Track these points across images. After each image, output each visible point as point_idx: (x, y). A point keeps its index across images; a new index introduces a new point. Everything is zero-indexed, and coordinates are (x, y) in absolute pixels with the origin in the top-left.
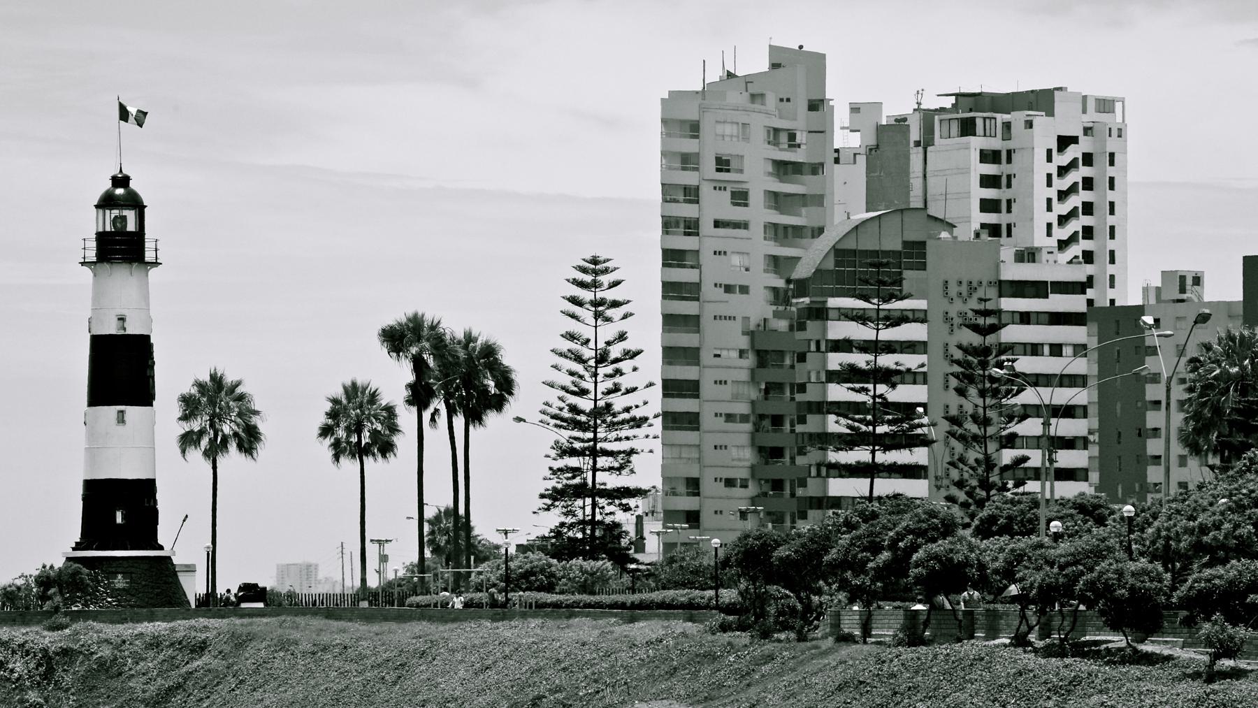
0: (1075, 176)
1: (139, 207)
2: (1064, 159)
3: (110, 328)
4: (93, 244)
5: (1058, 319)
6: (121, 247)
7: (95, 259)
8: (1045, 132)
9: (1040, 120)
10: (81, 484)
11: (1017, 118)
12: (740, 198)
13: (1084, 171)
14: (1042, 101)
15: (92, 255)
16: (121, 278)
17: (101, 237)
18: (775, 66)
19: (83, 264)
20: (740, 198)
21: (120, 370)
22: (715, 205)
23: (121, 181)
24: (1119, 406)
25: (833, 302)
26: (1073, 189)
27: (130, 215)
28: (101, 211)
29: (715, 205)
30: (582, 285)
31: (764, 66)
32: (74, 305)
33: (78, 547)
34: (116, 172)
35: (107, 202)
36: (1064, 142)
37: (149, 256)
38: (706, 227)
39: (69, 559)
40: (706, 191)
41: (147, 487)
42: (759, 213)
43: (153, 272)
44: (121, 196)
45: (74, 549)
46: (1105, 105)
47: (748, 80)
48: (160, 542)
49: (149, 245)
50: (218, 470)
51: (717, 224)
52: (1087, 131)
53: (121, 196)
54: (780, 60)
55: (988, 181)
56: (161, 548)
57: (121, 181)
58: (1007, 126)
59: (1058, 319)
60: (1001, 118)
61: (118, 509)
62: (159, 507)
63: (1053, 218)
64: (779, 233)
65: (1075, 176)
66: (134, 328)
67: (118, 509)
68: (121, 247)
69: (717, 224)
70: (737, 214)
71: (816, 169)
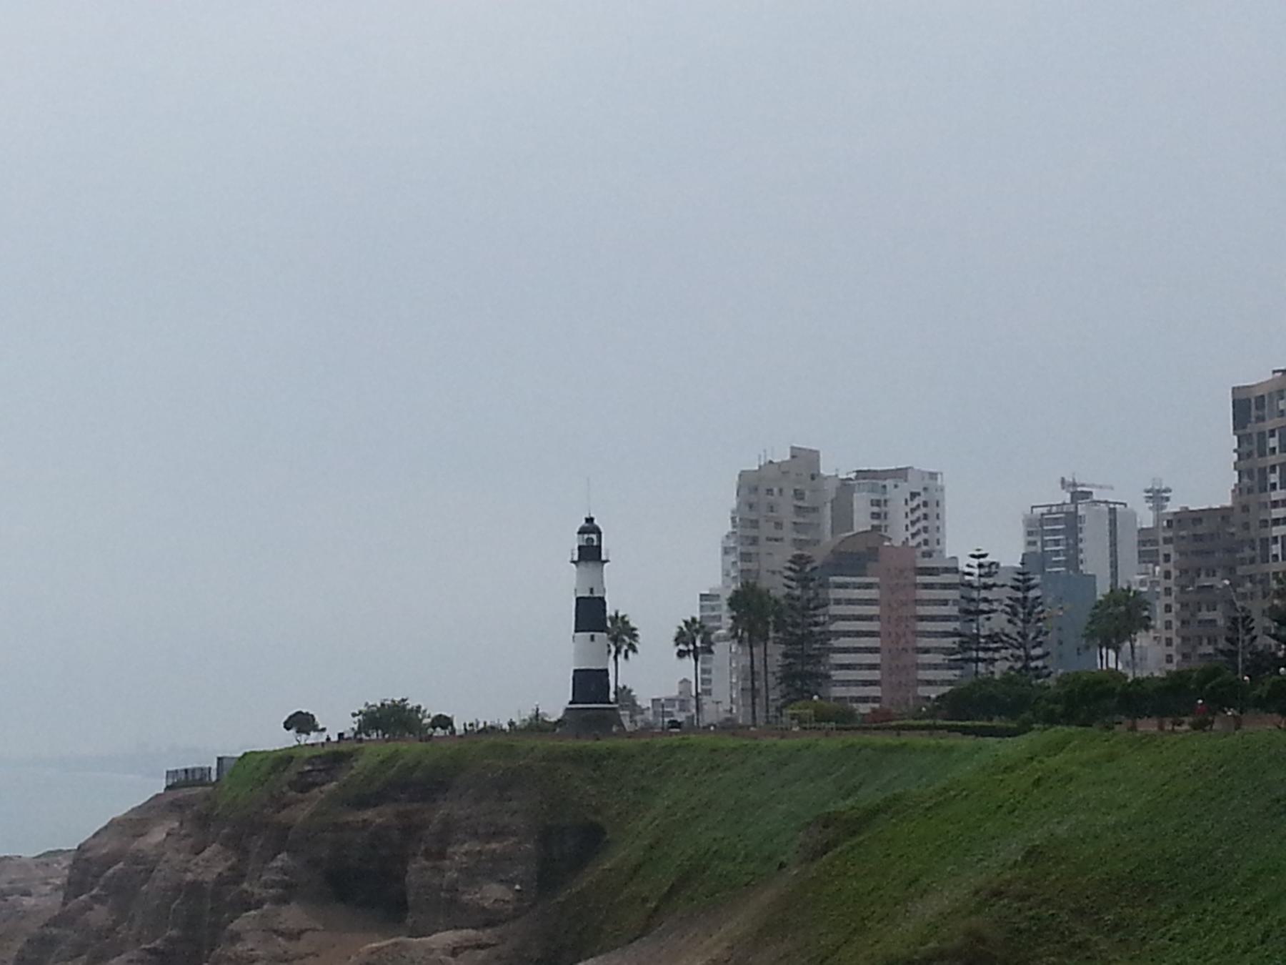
0: (919, 513)
1: (599, 533)
2: (914, 504)
4: (576, 552)
5: (945, 586)
6: (590, 554)
8: (905, 488)
9: (901, 484)
11: (889, 483)
12: (779, 525)
13: (923, 510)
14: (901, 474)
15: (576, 558)
18: (793, 457)
20: (779, 525)
21: (590, 613)
22: (767, 530)
23: (590, 520)
25: (832, 579)
26: (918, 520)
27: (594, 536)
29: (767, 530)
30: (1017, 580)
31: (788, 458)
32: (567, 584)
36: (913, 495)
37: (604, 558)
38: (762, 540)
40: (762, 522)
42: (788, 534)
43: (606, 565)
44: (590, 528)
46: (933, 476)
47: (779, 464)
51: (769, 539)
52: (925, 489)
53: (590, 528)
54: (796, 453)
55: (875, 516)
58: (884, 487)
59: (945, 586)
60: (881, 483)
63: (908, 535)
64: (798, 543)
65: (919, 513)
67: (590, 683)
68: (590, 554)
69: (769, 539)
70: (779, 534)
71: (815, 510)
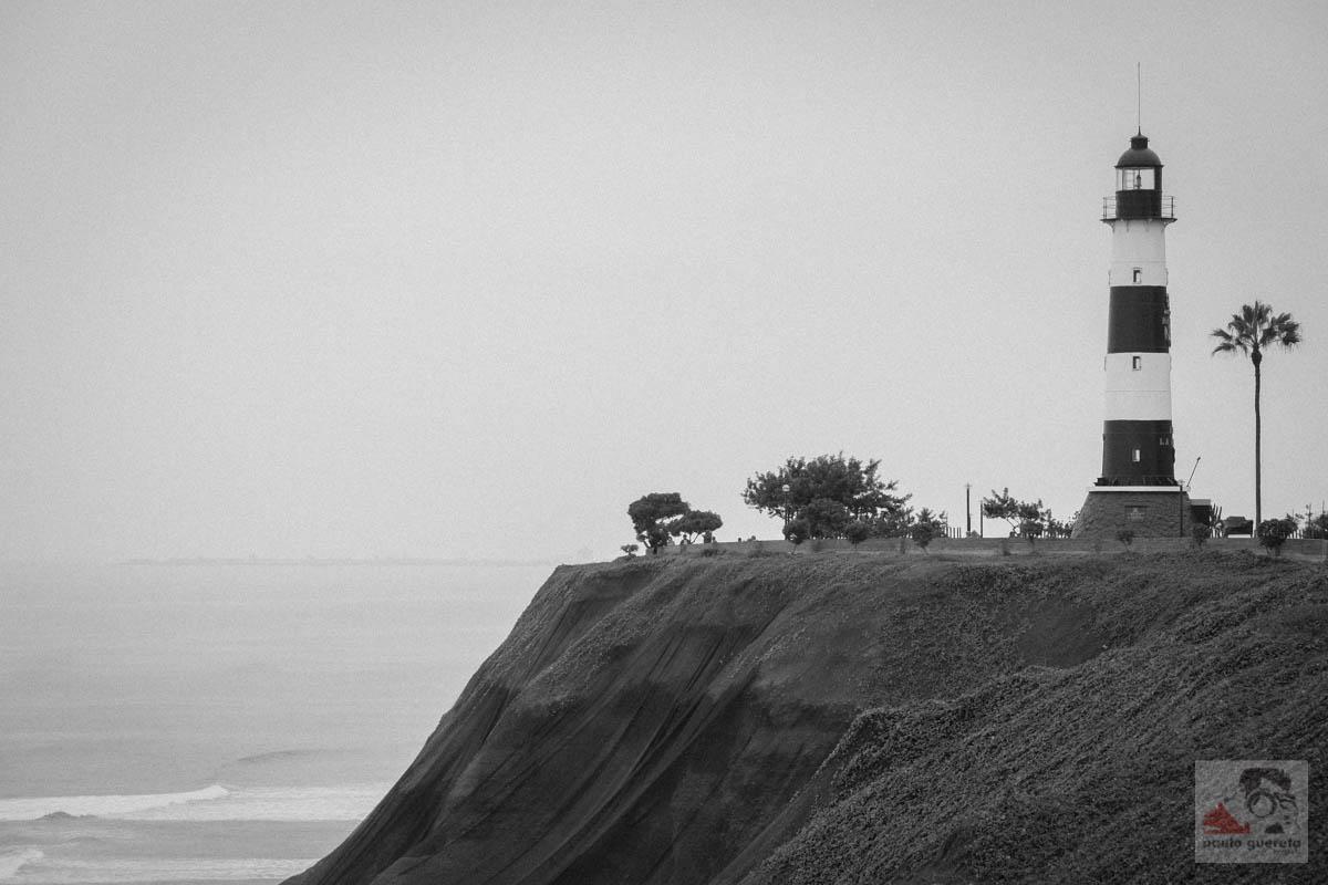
1: (1158, 168)
3: (1148, 359)
7: (1114, 216)
10: (1101, 430)
15: (1112, 213)
16: (1138, 232)
17: (1123, 196)
19: (1105, 220)
21: (1140, 320)
23: (1140, 143)
24: (857, 497)
28: (1121, 171)
33: (1101, 482)
34: (1135, 134)
35: (1125, 164)
37: (1165, 212)
39: (1091, 493)
41: (1163, 428)
43: (1170, 226)
44: (1139, 155)
45: (1097, 484)
48: (1176, 479)
49: (1165, 202)
50: (1255, 389)
53: (1139, 155)
56: (1175, 484)
57: (1140, 143)
61: (1140, 449)
62: (1175, 446)
66: (1148, 280)
67: (1140, 449)
68: (1141, 207)
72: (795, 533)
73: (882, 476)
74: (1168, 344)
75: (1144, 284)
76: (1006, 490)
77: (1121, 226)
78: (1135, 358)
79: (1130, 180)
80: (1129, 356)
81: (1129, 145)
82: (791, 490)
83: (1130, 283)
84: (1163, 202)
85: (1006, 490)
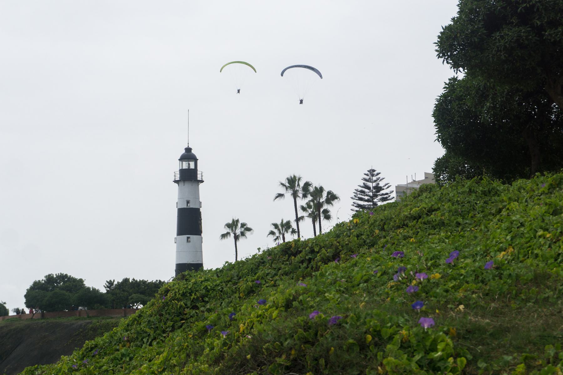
3: (193, 238)
6: (189, 176)
15: (178, 179)
16: (188, 186)
17: (182, 171)
23: (188, 150)
35: (183, 159)
37: (199, 178)
44: (188, 155)
53: (188, 155)
57: (188, 150)
66: (191, 206)
68: (189, 176)
72: (144, 306)
73: (69, 275)
74: (201, 232)
75: (191, 207)
76: (224, 236)
77: (181, 184)
78: (188, 238)
79: (185, 165)
80: (185, 237)
81: (184, 151)
82: (252, 338)
83: (185, 207)
84: (198, 172)
85: (224, 236)
